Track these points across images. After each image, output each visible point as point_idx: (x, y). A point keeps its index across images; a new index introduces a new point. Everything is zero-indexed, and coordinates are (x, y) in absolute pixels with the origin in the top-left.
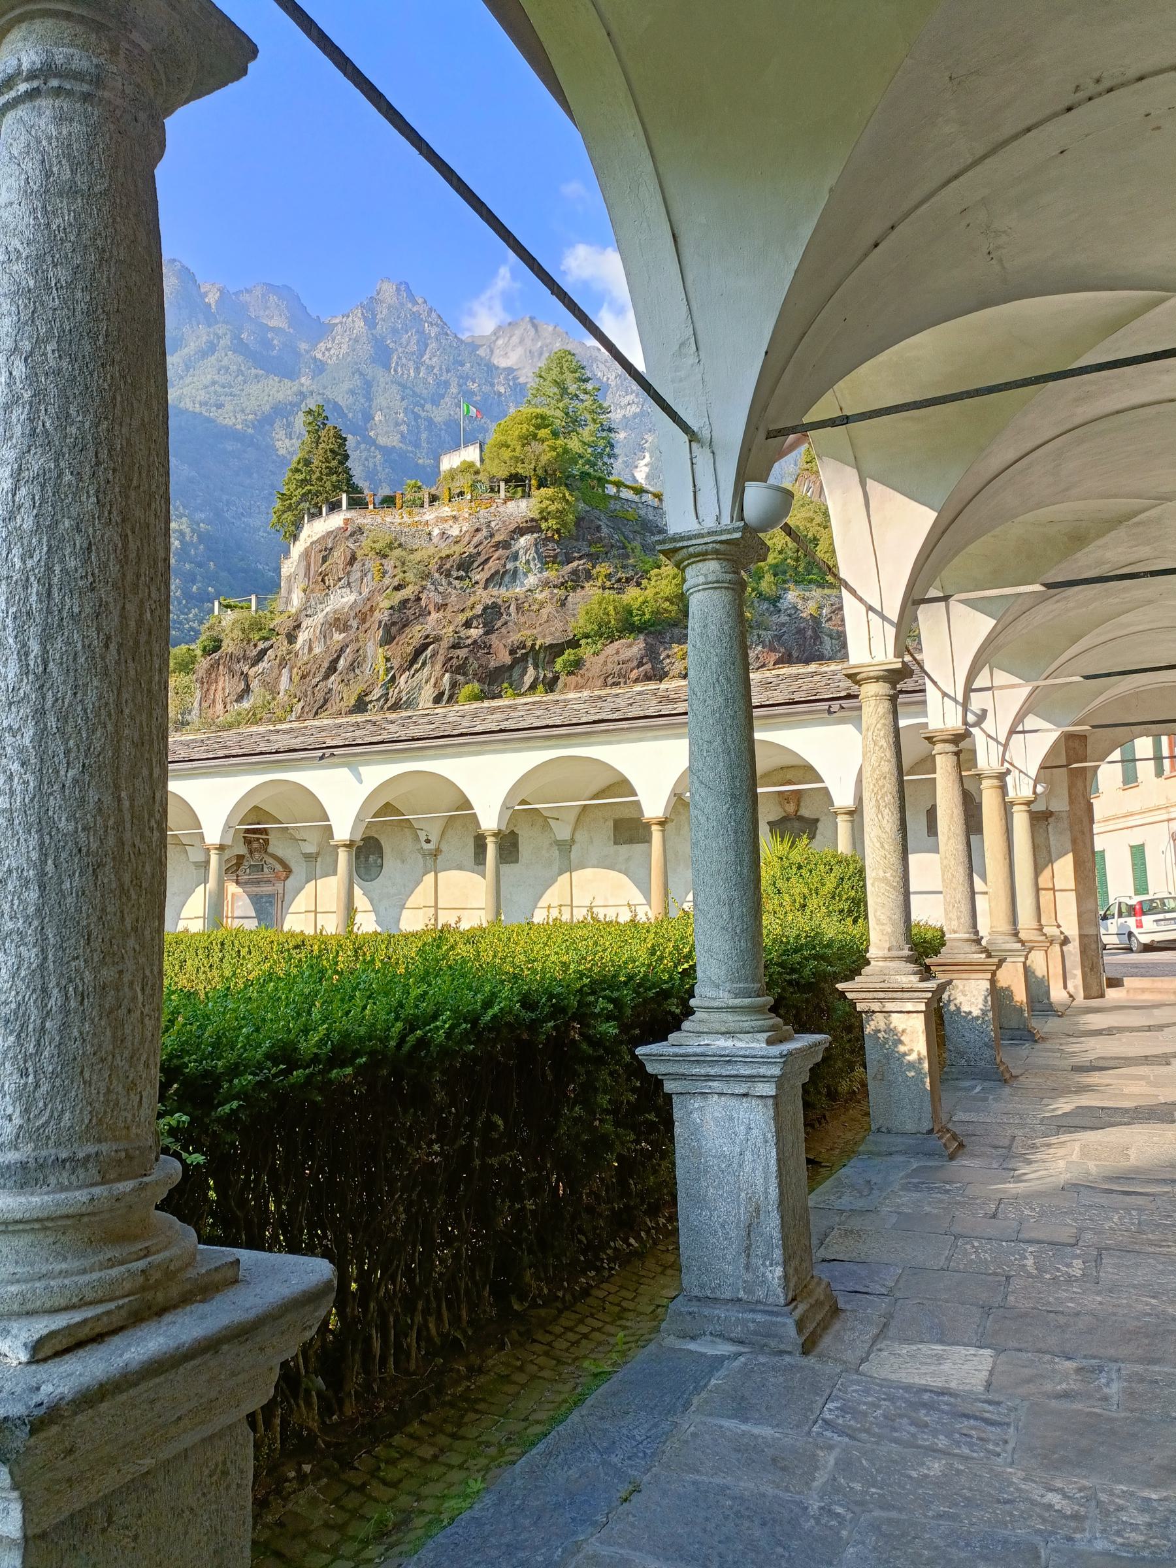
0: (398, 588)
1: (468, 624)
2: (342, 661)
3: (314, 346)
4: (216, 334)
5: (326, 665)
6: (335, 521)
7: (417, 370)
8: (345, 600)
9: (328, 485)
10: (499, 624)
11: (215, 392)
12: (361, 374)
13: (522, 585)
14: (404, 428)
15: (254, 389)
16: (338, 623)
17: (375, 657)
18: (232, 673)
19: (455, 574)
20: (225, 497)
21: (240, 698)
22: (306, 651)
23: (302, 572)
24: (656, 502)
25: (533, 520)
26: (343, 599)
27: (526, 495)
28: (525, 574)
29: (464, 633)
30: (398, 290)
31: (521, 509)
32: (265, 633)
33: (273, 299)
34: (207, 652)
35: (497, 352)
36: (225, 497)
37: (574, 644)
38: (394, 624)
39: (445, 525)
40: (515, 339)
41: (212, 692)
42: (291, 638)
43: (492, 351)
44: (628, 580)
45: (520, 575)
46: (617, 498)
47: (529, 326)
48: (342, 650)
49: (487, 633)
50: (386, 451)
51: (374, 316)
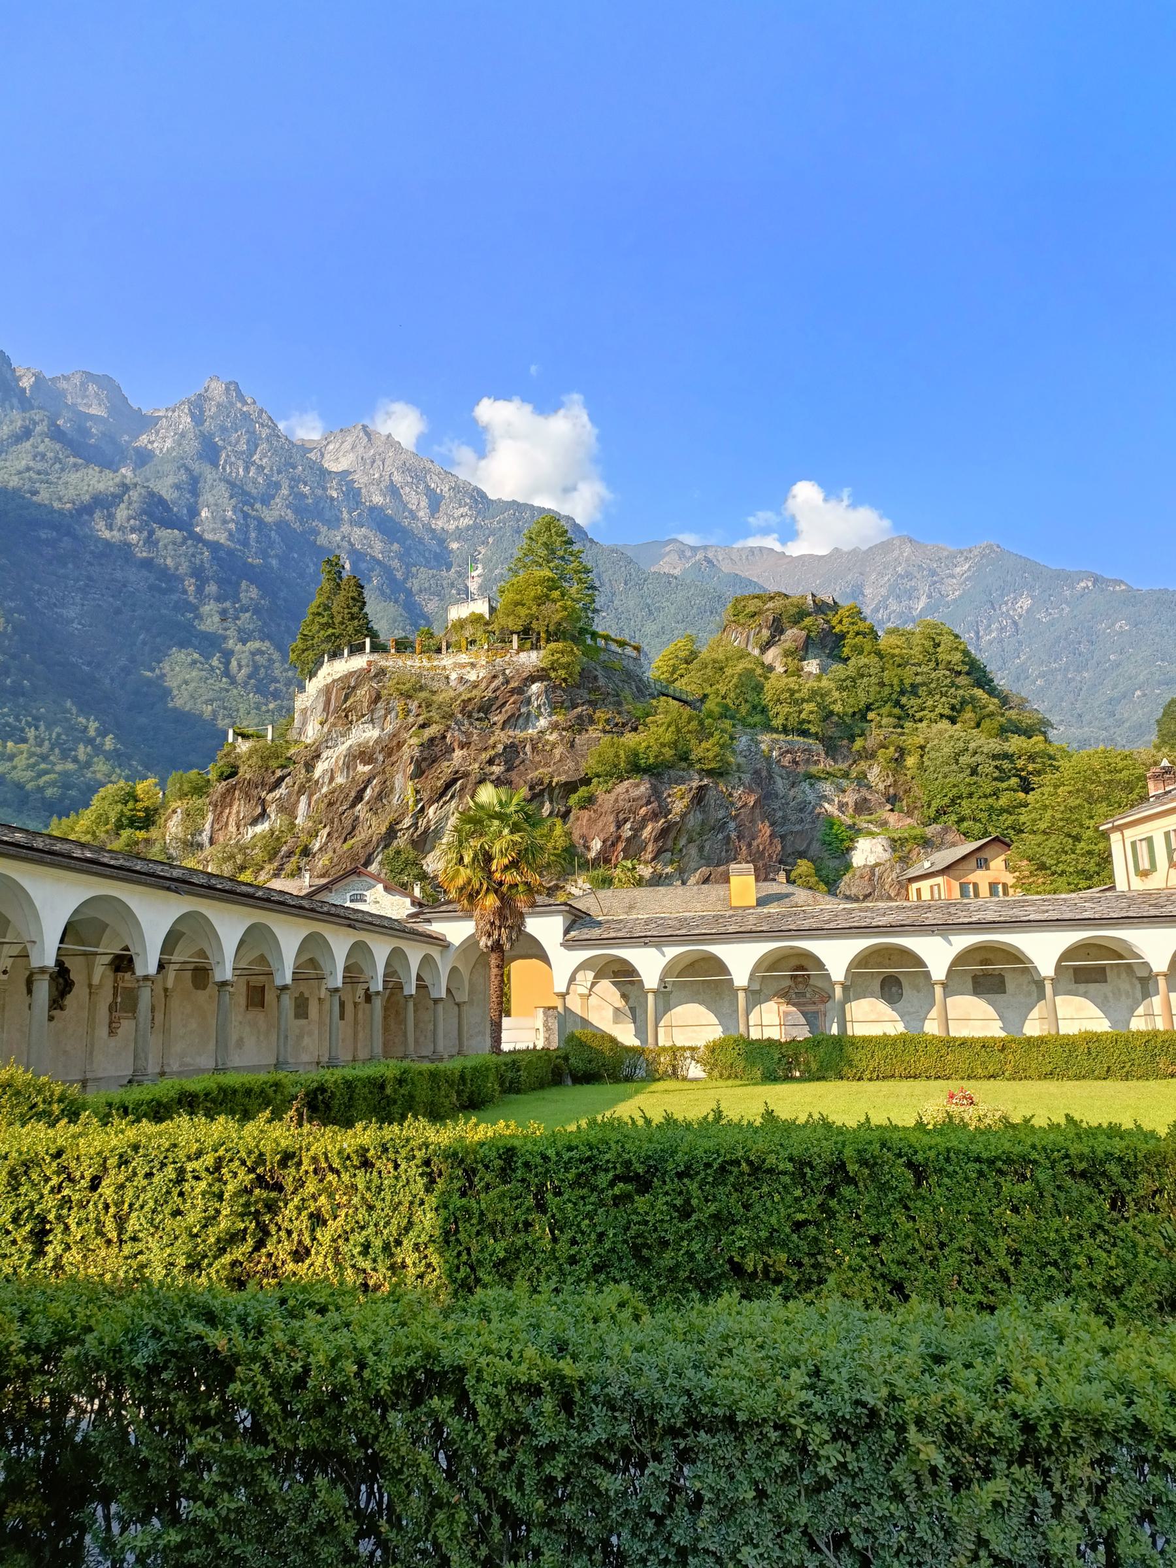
0: (423, 726)
1: (491, 762)
2: (368, 791)
3: (136, 438)
4: (31, 419)
5: (353, 794)
6: (359, 662)
7: (247, 470)
8: (368, 734)
9: (350, 630)
10: (517, 762)
11: (30, 479)
12: (187, 469)
13: (534, 727)
14: (232, 526)
15: (73, 477)
16: (363, 755)
17: (403, 791)
18: (248, 797)
19: (476, 715)
20: (37, 587)
21: (255, 822)
22: (326, 780)
23: (320, 707)
24: (634, 654)
25: (543, 669)
26: (366, 734)
27: (535, 647)
28: (537, 718)
29: (488, 769)
30: (227, 389)
31: (531, 659)
32: (282, 761)
33: (92, 388)
34: (223, 777)
35: (327, 457)
36: (37, 587)
37: (586, 781)
38: (424, 759)
39: (463, 670)
40: (347, 446)
41: (225, 815)
42: (309, 767)
43: (322, 455)
44: (624, 725)
45: (533, 718)
46: (607, 650)
47: (362, 434)
48: (369, 781)
49: (507, 770)
50: (214, 547)
51: (202, 412)
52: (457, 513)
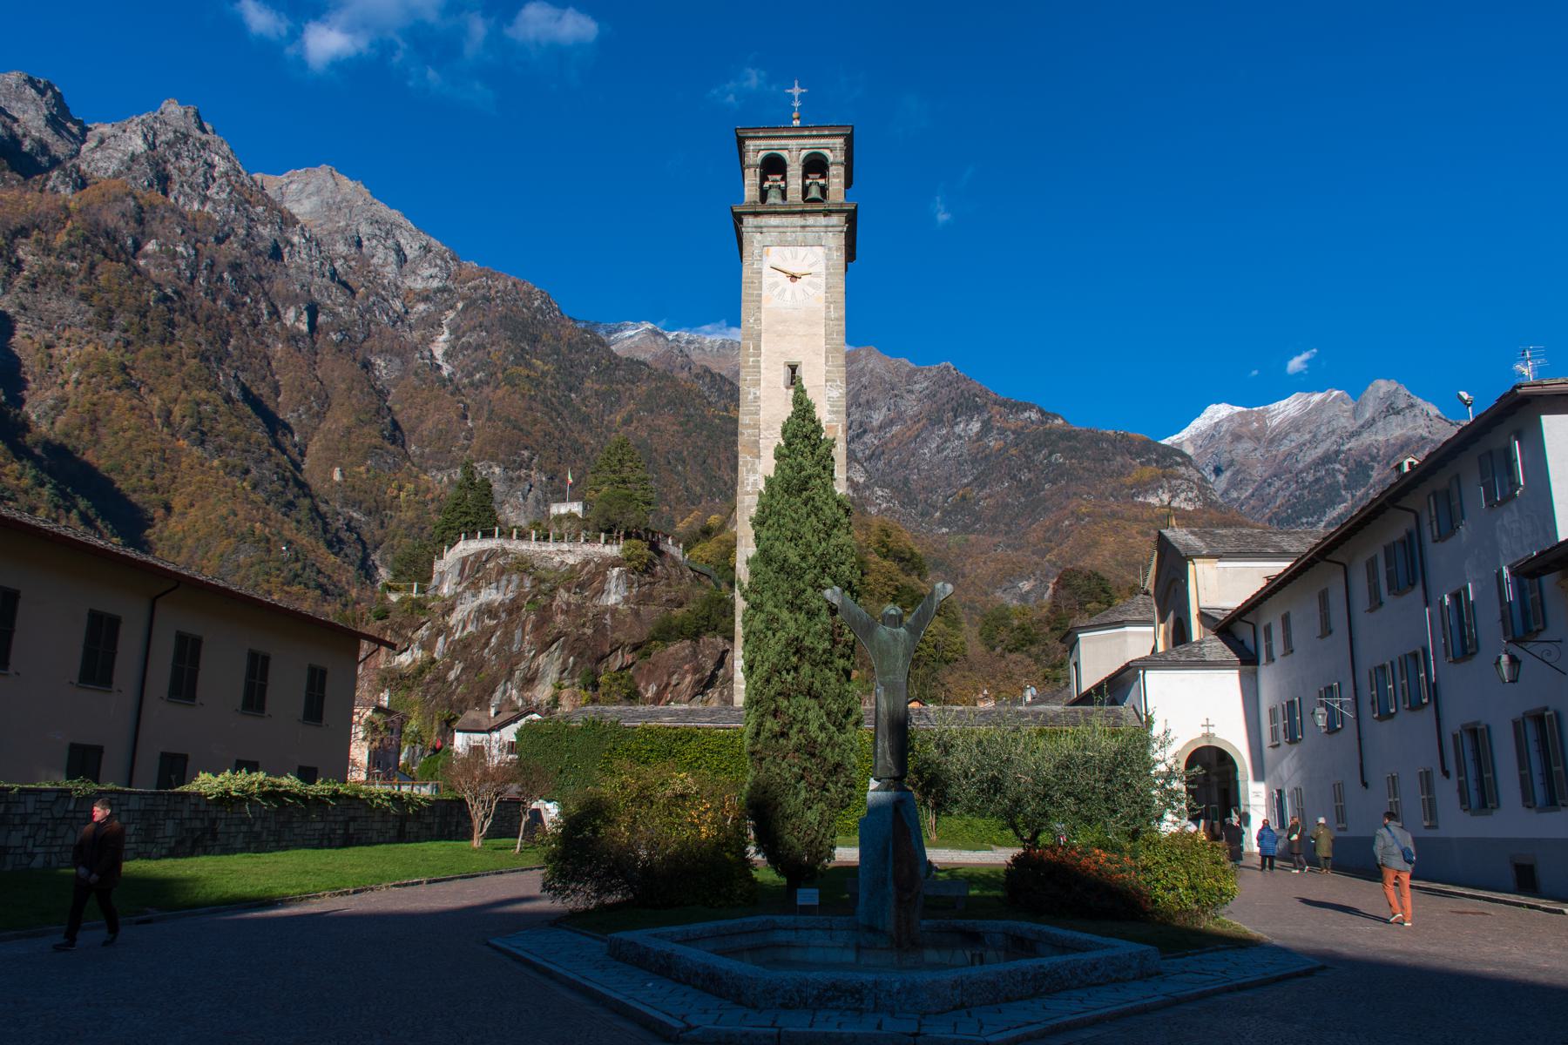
6: (489, 544)
16: (488, 611)
26: (490, 595)
31: (613, 550)
52: (427, 273)
